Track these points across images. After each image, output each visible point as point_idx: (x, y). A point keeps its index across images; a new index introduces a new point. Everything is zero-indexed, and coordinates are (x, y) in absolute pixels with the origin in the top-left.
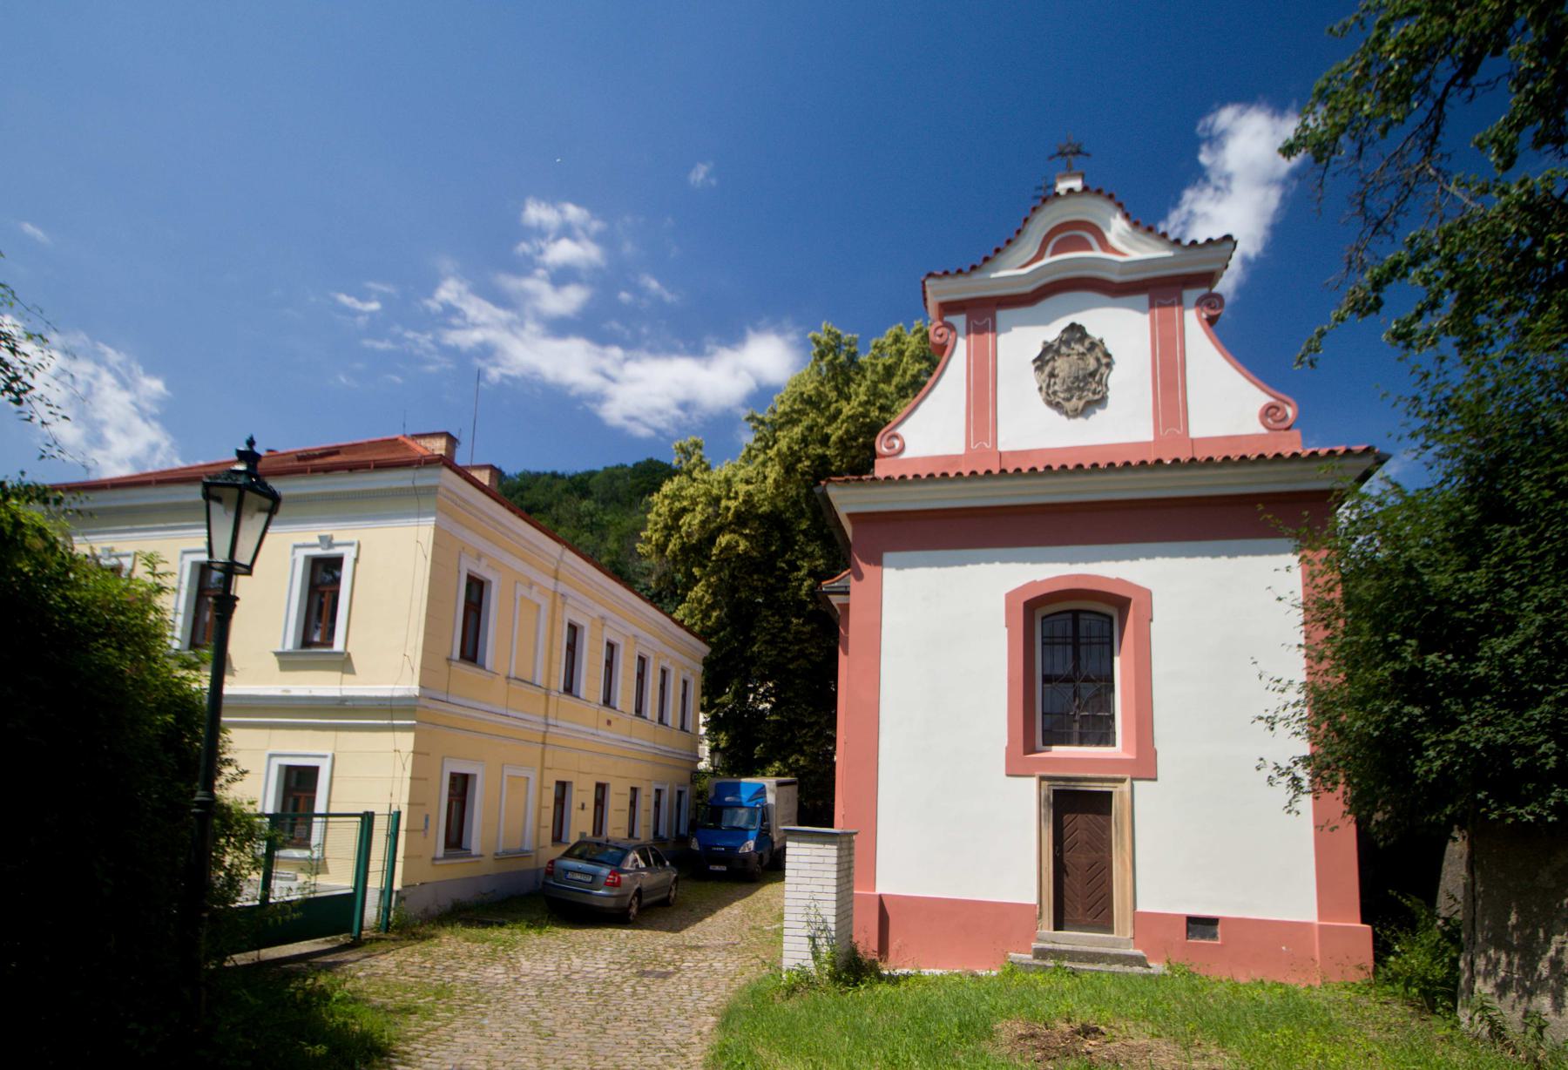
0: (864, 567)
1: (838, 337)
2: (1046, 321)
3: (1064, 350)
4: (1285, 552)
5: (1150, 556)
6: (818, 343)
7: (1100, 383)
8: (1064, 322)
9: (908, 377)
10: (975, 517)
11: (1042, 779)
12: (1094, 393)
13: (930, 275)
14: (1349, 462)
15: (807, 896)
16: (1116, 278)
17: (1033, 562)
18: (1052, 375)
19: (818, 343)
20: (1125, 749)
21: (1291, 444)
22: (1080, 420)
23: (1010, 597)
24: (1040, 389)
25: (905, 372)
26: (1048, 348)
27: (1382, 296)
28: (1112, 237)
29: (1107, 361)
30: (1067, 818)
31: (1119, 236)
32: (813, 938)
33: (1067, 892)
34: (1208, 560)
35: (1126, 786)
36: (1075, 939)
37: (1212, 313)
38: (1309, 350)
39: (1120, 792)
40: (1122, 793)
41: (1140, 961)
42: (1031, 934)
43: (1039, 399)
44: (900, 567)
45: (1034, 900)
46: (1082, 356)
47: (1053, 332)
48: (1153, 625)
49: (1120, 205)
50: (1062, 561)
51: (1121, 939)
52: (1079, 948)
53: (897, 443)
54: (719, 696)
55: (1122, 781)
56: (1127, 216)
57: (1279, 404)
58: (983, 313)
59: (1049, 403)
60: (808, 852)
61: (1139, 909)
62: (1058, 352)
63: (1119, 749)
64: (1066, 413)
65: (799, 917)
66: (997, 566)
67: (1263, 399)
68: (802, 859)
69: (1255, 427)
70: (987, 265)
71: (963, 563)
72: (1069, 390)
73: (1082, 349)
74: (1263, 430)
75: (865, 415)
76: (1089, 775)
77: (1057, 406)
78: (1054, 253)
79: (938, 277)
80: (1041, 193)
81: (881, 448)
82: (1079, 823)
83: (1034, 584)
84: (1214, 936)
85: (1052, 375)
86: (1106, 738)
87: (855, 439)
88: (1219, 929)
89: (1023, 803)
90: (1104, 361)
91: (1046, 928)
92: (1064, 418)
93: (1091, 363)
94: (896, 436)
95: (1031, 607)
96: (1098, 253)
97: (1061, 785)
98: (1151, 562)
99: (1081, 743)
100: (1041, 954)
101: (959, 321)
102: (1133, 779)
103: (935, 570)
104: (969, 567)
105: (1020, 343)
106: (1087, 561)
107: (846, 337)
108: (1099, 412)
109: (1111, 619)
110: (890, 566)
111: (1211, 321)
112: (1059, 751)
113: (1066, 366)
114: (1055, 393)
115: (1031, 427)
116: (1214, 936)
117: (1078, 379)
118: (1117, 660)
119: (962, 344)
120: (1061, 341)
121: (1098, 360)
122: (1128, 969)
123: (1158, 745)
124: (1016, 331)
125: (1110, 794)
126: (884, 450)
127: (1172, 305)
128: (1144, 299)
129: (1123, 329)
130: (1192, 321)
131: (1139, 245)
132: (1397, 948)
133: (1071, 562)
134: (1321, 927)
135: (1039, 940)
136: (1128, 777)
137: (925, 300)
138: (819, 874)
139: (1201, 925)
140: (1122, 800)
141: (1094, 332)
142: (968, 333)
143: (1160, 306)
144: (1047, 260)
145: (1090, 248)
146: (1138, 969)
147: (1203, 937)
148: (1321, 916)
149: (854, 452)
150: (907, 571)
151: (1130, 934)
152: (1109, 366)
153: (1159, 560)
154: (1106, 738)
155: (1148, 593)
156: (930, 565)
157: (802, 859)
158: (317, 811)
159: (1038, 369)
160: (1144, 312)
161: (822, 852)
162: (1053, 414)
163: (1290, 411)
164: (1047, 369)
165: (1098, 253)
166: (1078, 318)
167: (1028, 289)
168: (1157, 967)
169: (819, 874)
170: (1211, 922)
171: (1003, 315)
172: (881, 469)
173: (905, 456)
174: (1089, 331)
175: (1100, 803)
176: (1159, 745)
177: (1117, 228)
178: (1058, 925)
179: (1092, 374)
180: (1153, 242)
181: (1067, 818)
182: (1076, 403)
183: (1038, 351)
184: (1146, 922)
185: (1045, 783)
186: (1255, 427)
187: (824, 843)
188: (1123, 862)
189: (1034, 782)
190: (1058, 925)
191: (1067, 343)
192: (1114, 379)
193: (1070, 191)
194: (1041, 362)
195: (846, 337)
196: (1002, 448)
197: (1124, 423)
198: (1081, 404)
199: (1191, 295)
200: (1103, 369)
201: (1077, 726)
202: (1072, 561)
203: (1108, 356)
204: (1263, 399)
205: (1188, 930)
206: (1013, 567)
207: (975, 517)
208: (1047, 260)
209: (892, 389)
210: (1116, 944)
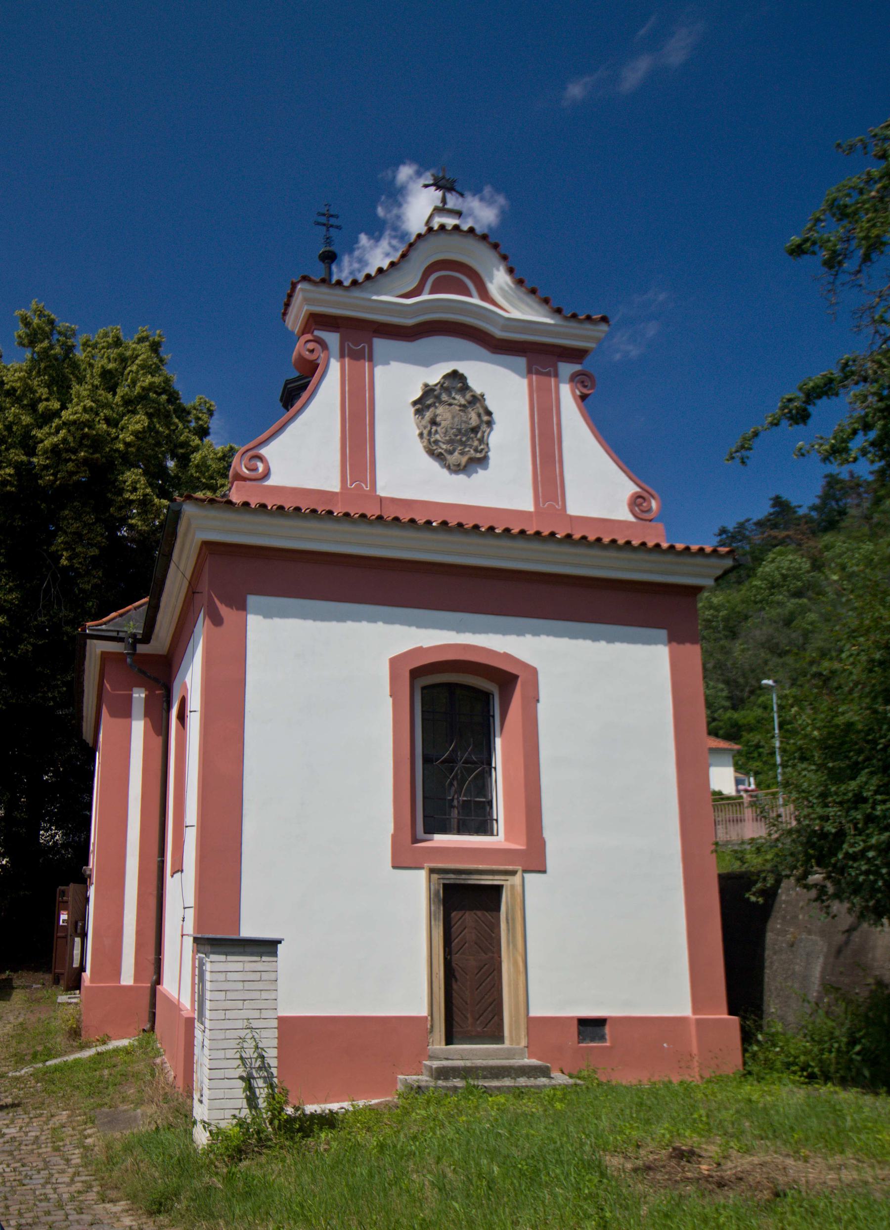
0: (224, 610)
1: (51, 322)
2: (426, 362)
3: (444, 397)
4: (656, 642)
5: (536, 633)
6: (27, 324)
7: (481, 441)
8: (446, 368)
9: (138, 389)
10: (352, 564)
11: (432, 871)
12: (476, 450)
13: (305, 279)
14: (713, 561)
15: (239, 1024)
16: (498, 333)
17: (419, 626)
18: (434, 422)
19: (27, 324)
20: (507, 838)
21: (656, 536)
22: (461, 477)
23: (395, 663)
24: (421, 435)
25: (134, 383)
26: (428, 391)
27: (810, 409)
28: (493, 289)
29: (488, 418)
31: (501, 289)
32: (248, 1080)
33: (457, 1000)
34: (588, 643)
35: (516, 880)
36: (471, 1053)
37: (586, 391)
38: (742, 447)
40: (513, 886)
41: (544, 1072)
42: (423, 1052)
43: (419, 447)
44: (268, 615)
45: (424, 1012)
46: (464, 408)
47: (435, 375)
48: (540, 706)
49: (504, 258)
50: (441, 628)
51: (513, 1047)
52: (479, 1062)
53: (261, 467)
55: (513, 873)
56: (511, 271)
57: (645, 495)
58: (363, 335)
59: (431, 453)
60: (239, 966)
61: (533, 1013)
62: (438, 398)
63: (498, 839)
64: (449, 468)
65: (231, 1054)
66: (380, 627)
67: (631, 488)
68: (231, 976)
70: (368, 284)
71: (341, 619)
72: (450, 442)
73: (463, 402)
74: (631, 518)
75: (90, 424)
76: (481, 867)
77: (439, 457)
78: (431, 293)
79: (314, 283)
80: (323, 220)
82: (468, 919)
83: (419, 651)
84: (602, 1038)
85: (434, 422)
86: (484, 826)
87: (75, 451)
88: (607, 1029)
89: (412, 895)
90: (485, 418)
91: (438, 1044)
92: (445, 472)
93: (474, 421)
94: (260, 458)
95: (416, 673)
96: (476, 301)
97: (452, 879)
98: (537, 638)
99: (459, 832)
100: (443, 1073)
101: (332, 339)
102: (525, 871)
103: (309, 623)
104: (350, 624)
105: (400, 381)
106: (474, 632)
107: (62, 325)
108: (481, 472)
110: (257, 613)
111: (583, 397)
112: (441, 840)
113: (448, 415)
114: (436, 442)
115: (407, 473)
116: (602, 1038)
118: (498, 742)
119: (335, 367)
120: (441, 385)
121: (479, 415)
122: (532, 1082)
124: (394, 365)
125: (498, 889)
127: (548, 374)
128: (522, 362)
129: (503, 388)
130: (566, 394)
131: (523, 306)
132: (760, 1037)
133: (459, 631)
134: (697, 1020)
135: (431, 1058)
136: (519, 868)
137: (287, 305)
138: (256, 995)
139: (591, 1027)
140: (513, 894)
141: (476, 384)
142: (342, 356)
143: (538, 373)
144: (425, 297)
145: (470, 295)
146: (543, 1081)
147: (593, 1040)
148: (695, 1010)
149: (70, 465)
150: (277, 621)
151: (523, 1043)
152: (490, 424)
153: (543, 638)
154: (484, 826)
155: (534, 672)
156: (304, 616)
157: (231, 976)
158: (192, 910)
159: (418, 412)
160: (523, 377)
161: (259, 966)
162: (434, 465)
163: (654, 504)
164: (428, 415)
165: (476, 301)
166: (463, 367)
167: (410, 321)
168: (560, 1079)
169: (256, 995)
170: (600, 1022)
171: (380, 345)
173: (270, 482)
174: (471, 383)
175: (486, 898)
176: (548, 834)
177: (499, 280)
178: (449, 1041)
179: (475, 430)
180: (536, 306)
183: (418, 394)
184: (537, 1025)
185: (435, 877)
187: (261, 955)
188: (515, 963)
189: (422, 874)
190: (449, 1041)
191: (447, 390)
192: (495, 439)
193: (442, 227)
194: (421, 405)
195: (62, 325)
196: (381, 492)
197: (503, 487)
198: (464, 460)
199: (567, 369)
200: (484, 427)
201: (455, 812)
202: (459, 630)
203: (489, 413)
204: (631, 488)
205: (579, 1033)
206: (398, 629)
207: (352, 564)
208: (425, 297)
209: (118, 399)
210: (510, 1054)
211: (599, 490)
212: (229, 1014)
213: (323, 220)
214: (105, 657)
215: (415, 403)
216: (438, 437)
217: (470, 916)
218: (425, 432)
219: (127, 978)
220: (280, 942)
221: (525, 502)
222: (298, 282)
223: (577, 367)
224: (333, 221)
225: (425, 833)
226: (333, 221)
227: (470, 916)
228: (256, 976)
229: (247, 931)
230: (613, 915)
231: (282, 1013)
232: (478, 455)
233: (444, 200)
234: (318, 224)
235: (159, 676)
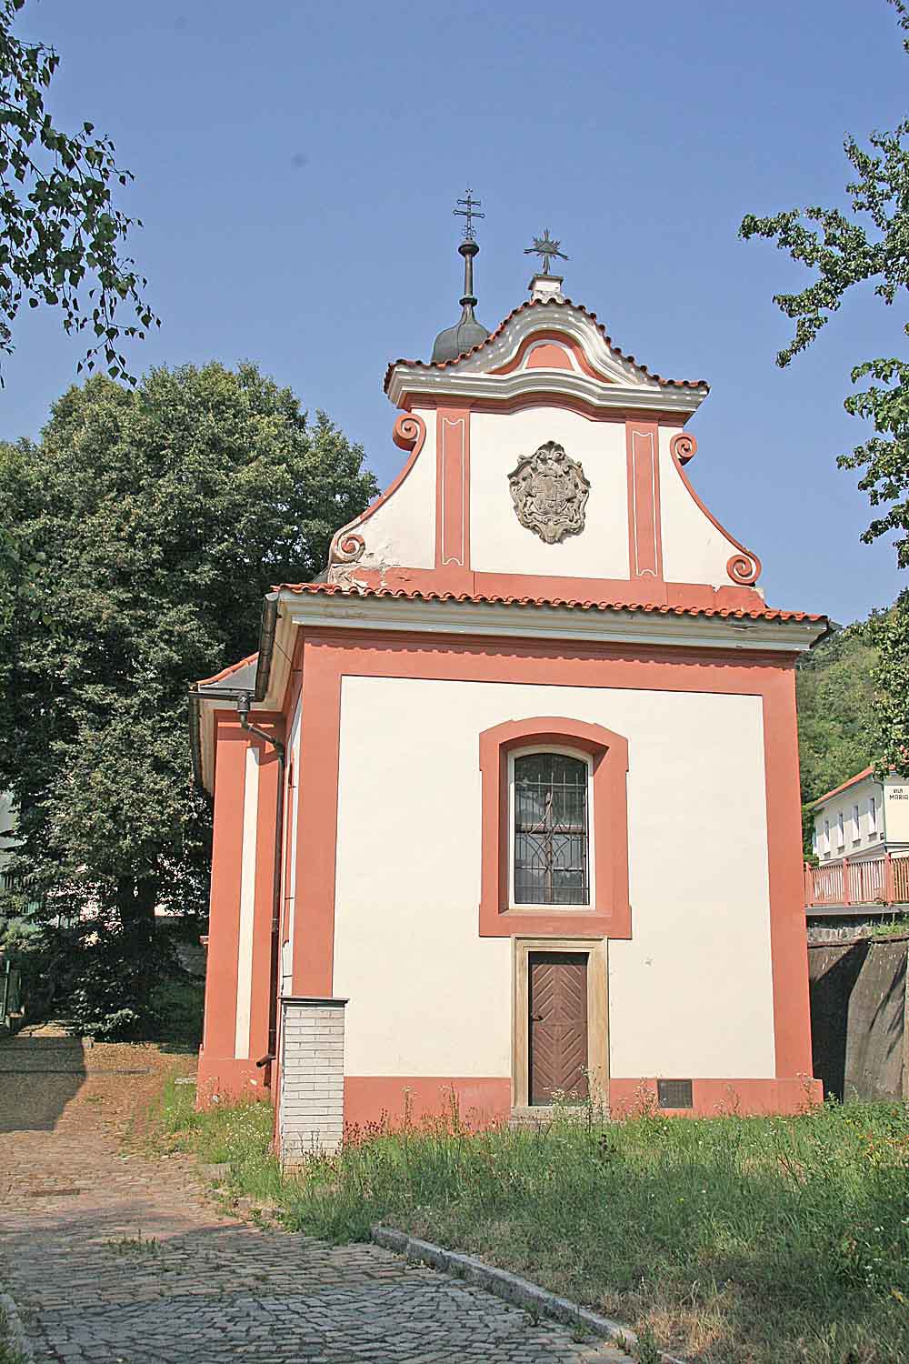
23: (484, 737)
24: (516, 507)
30: (534, 966)
39: (595, 950)
40: (598, 954)
43: (513, 518)
54: (38, 802)
68: (304, 1031)
69: (720, 579)
80: (464, 208)
81: (336, 549)
86: (585, 902)
89: (501, 962)
95: (506, 747)
109: (585, 765)
115: (503, 546)
117: (551, 494)
123: (591, 722)
126: (341, 554)
129: (601, 450)
154: (585, 902)
157: (304, 1031)
172: (335, 577)
181: (534, 966)
182: (551, 529)
186: (720, 579)
196: (476, 566)
197: (597, 555)
203: (588, 483)
211: (696, 555)
212: (303, 1062)
213: (464, 208)
214: (219, 715)
215: (510, 476)
216: (533, 508)
217: (557, 991)
218: (521, 505)
219: (242, 1050)
220: (346, 1002)
221: (621, 571)
222: (395, 366)
223: (677, 431)
224: (474, 209)
225: (516, 903)
226: (474, 209)
227: (557, 991)
228: (326, 1031)
229: (337, 995)
230: (695, 998)
231: (354, 1069)
232: (574, 525)
233: (546, 265)
234: (457, 213)
235: (271, 731)
